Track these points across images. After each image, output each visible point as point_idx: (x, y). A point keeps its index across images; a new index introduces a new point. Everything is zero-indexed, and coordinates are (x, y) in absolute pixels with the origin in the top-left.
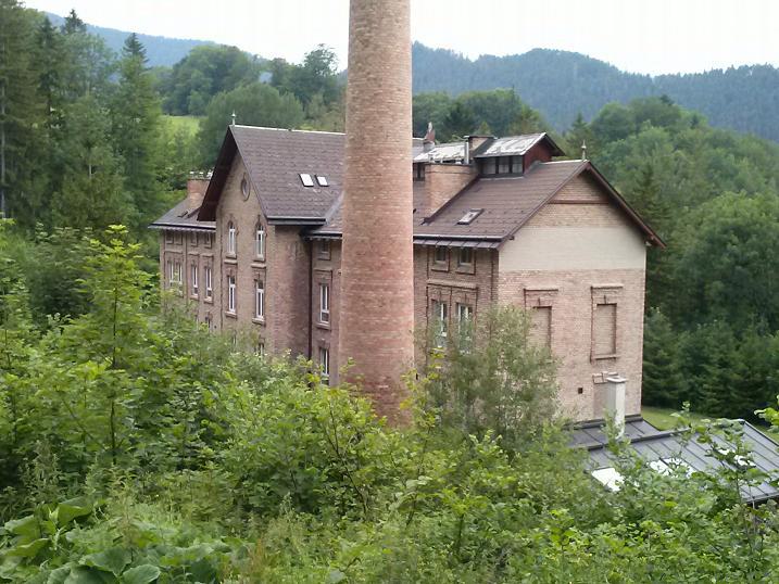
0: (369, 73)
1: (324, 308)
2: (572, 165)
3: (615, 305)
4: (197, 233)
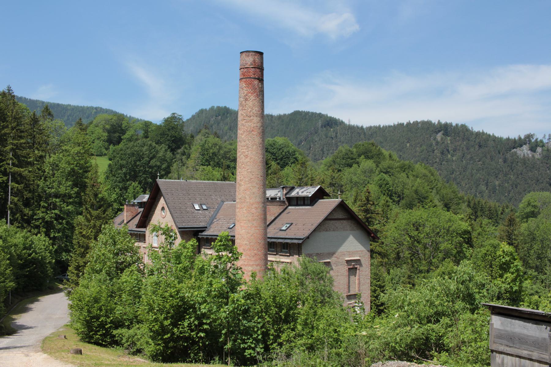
0: (248, 170)
2: (334, 202)
4: (140, 234)
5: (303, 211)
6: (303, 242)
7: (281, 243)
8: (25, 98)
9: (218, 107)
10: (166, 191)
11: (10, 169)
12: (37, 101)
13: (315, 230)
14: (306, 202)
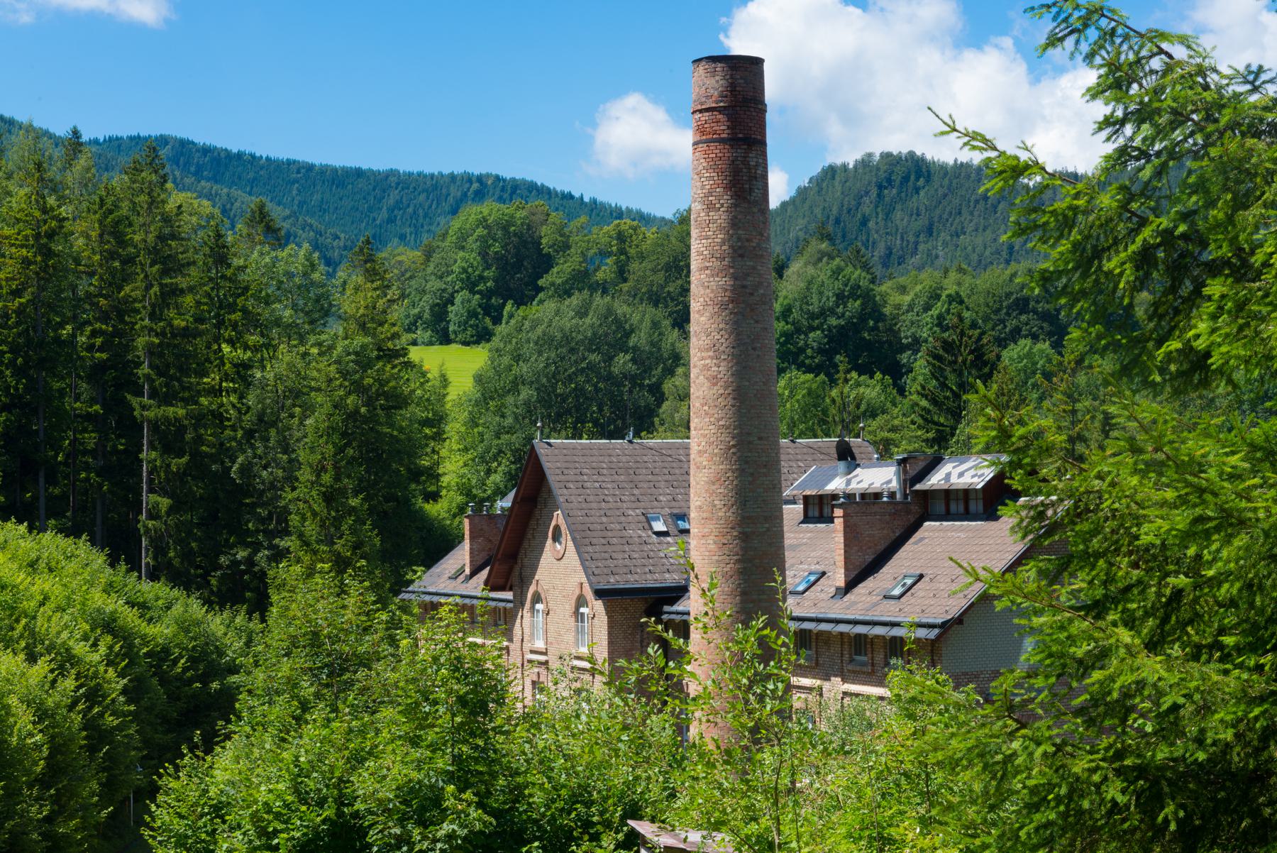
5: (962, 535)
6: (939, 637)
8: (253, 156)
9: (887, 156)
10: (563, 478)
11: (144, 407)
12: (290, 163)
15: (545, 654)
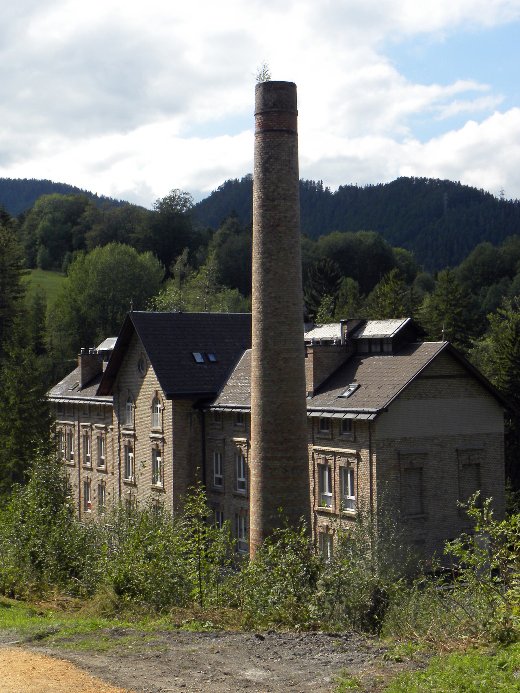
0: (270, 293)
1: (217, 473)
2: (435, 346)
3: (478, 465)
7: (317, 418)
13: (398, 397)
14: (385, 348)
15: (162, 433)
